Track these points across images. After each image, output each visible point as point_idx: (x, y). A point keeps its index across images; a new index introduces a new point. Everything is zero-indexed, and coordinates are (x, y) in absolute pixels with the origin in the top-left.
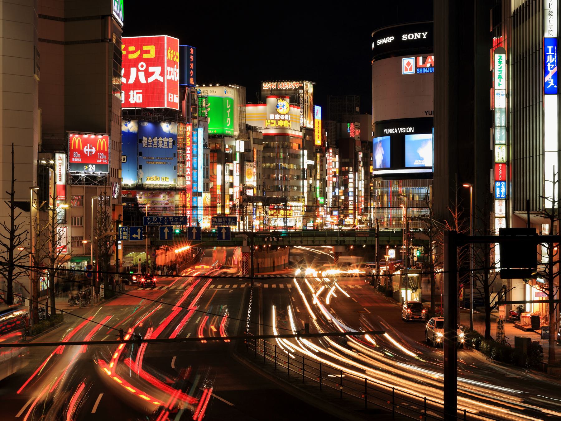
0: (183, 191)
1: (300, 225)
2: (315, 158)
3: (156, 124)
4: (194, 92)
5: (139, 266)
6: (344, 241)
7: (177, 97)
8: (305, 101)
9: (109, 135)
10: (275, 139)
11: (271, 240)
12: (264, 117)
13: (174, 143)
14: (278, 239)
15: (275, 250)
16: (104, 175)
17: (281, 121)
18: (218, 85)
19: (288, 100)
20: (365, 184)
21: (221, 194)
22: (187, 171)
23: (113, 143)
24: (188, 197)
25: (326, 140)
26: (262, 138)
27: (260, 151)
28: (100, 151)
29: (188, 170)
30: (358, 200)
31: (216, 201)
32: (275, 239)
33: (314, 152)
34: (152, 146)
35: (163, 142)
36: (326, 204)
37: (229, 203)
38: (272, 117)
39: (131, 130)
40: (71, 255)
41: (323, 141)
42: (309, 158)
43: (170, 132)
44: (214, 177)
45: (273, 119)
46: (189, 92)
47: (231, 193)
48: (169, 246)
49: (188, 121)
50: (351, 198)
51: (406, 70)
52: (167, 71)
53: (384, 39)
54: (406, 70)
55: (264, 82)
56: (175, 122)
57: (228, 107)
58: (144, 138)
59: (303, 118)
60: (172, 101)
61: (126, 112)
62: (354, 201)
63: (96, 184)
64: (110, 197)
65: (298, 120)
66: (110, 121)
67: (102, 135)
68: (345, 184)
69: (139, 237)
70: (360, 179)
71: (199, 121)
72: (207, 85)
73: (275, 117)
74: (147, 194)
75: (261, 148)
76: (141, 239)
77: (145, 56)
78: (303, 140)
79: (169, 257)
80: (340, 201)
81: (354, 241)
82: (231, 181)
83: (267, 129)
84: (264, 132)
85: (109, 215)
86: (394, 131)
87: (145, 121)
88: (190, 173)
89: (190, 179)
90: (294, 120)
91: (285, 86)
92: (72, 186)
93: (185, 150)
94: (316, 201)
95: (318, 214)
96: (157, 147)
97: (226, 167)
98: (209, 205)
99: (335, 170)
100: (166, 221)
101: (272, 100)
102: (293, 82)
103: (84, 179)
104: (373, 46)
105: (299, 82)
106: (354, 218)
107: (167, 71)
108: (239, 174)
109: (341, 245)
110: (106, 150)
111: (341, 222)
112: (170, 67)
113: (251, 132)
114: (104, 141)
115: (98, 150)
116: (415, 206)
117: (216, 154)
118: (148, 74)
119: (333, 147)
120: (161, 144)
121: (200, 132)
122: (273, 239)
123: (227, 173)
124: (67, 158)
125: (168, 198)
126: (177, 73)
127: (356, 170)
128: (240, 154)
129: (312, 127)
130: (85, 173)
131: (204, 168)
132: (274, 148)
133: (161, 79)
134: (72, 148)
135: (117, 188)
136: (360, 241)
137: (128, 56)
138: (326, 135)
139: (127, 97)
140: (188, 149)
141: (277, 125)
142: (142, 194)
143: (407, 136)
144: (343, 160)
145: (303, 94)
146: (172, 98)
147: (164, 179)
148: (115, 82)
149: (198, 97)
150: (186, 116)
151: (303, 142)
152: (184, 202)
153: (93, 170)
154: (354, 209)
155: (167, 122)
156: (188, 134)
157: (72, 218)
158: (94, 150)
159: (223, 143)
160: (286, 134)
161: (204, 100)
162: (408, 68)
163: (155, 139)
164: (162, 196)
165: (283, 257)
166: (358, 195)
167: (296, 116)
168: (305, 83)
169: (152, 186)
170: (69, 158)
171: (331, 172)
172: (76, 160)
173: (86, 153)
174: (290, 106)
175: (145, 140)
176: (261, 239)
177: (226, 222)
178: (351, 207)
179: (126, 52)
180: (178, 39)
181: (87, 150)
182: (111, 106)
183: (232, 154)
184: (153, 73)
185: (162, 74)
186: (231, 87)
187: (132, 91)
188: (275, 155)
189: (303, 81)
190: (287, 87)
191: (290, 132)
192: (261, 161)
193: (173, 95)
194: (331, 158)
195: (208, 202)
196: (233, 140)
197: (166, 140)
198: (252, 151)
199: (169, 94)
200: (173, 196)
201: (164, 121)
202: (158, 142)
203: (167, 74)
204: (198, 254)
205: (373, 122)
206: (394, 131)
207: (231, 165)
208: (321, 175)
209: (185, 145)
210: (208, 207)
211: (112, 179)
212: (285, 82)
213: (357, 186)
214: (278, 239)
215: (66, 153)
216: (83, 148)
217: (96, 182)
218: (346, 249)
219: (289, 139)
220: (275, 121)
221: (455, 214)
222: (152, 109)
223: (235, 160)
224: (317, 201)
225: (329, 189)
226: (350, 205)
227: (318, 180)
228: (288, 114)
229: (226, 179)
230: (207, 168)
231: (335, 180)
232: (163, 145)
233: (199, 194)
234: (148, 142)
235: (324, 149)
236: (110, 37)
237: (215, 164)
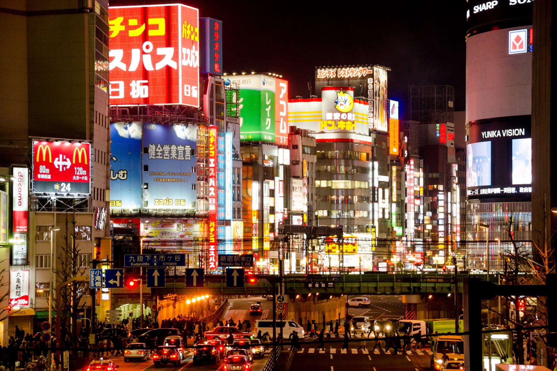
0: (207, 218)
1: (368, 266)
2: (389, 173)
3: (167, 125)
4: (220, 83)
5: (130, 322)
6: (419, 288)
7: (196, 89)
8: (376, 94)
9: (90, 142)
10: (333, 146)
11: (317, 285)
12: (319, 117)
13: (193, 152)
14: (327, 285)
15: (326, 300)
16: (83, 197)
17: (341, 121)
18: (253, 73)
19: (352, 93)
20: (461, 208)
21: (258, 222)
22: (210, 191)
23: (97, 153)
24: (212, 226)
25: (405, 147)
26: (315, 146)
27: (312, 163)
28: (77, 164)
29: (212, 189)
30: (451, 230)
31: (251, 232)
32: (323, 285)
33: (388, 165)
34: (161, 157)
35: (177, 152)
36: (406, 236)
37: (268, 235)
38: (329, 116)
39: (133, 136)
40: (35, 309)
41: (401, 149)
42: (382, 172)
43: (186, 138)
44: (249, 199)
45: (331, 119)
46: (213, 83)
47: (272, 221)
48: (178, 294)
49: (212, 122)
50: (441, 228)
51: (515, 47)
52: (182, 54)
53: (484, 5)
54: (515, 47)
55: (318, 68)
56: (193, 124)
57: (268, 103)
58: (150, 146)
59: (373, 117)
60: (189, 95)
61: (126, 111)
62: (446, 232)
63: (71, 210)
64: (91, 227)
65: (365, 121)
66: (92, 122)
67: (80, 142)
68: (433, 207)
69: (118, 283)
70: (455, 201)
71: (227, 123)
72: (239, 74)
73: (333, 117)
74: (155, 223)
75: (314, 159)
76: (121, 286)
77: (151, 33)
78: (373, 148)
79: (179, 310)
80: (426, 231)
81: (434, 288)
82: (272, 205)
83: (323, 132)
84: (318, 137)
85: (79, 252)
86: (496, 134)
87: (152, 123)
88: (214, 194)
89: (214, 203)
90: (360, 120)
91: (347, 73)
92: (37, 212)
93: (207, 162)
94: (392, 232)
95: (395, 250)
96: (168, 158)
97: (264, 185)
98: (242, 237)
99: (418, 189)
100: (155, 261)
101: (329, 94)
102: (358, 67)
103: (55, 204)
104: (468, 15)
105: (367, 67)
106: (447, 255)
107: (182, 54)
108: (283, 195)
109: (414, 293)
110: (86, 163)
111: (427, 261)
112: (187, 48)
113: (298, 137)
114: (83, 151)
115: (74, 162)
116: (527, 239)
117: (250, 168)
118: (156, 58)
119: (416, 157)
120: (174, 155)
121: (229, 136)
122: (320, 285)
123: (266, 193)
124: (30, 174)
125: (184, 229)
126: (196, 57)
127: (448, 189)
128: (284, 167)
129: (385, 129)
130: (56, 194)
131: (234, 188)
132: (332, 159)
134: (38, 160)
135: (104, 214)
136: (442, 288)
137: (128, 33)
138: (406, 141)
139: (128, 89)
140: (212, 160)
141: (336, 128)
142: (148, 223)
143: (514, 141)
144: (430, 175)
145: (373, 84)
146: (189, 90)
147: (179, 201)
148: (99, 66)
149: (226, 90)
150: (208, 116)
151: (372, 151)
152: (206, 233)
153: (67, 191)
154: (446, 242)
155: (183, 125)
156: (212, 140)
157: (37, 257)
158: (68, 164)
159: (260, 153)
160: (349, 139)
161: (234, 95)
162: (518, 45)
163: (166, 148)
164: (175, 225)
165: (337, 309)
166: (451, 224)
167: (363, 114)
168: (375, 68)
169: (162, 212)
170: (34, 174)
171: (412, 191)
172: (43, 176)
173: (57, 167)
174: (355, 101)
175: (152, 149)
176: (303, 285)
177: (238, 262)
178: (441, 240)
179: (126, 28)
180: (198, 10)
181: (58, 163)
182: (93, 103)
183: (273, 168)
185: (175, 58)
186: (271, 75)
187: (133, 82)
188: (333, 169)
189: (372, 66)
190: (351, 75)
191: (353, 137)
192: (314, 176)
193: (191, 87)
194: (412, 172)
195: (240, 235)
196: (274, 149)
197: (181, 148)
198: (301, 164)
199: (186, 86)
200: (191, 225)
201: (179, 122)
202: (170, 152)
203: (182, 58)
204: (223, 306)
205: (467, 122)
206: (496, 134)
207: (271, 182)
208: (398, 196)
209: (208, 156)
210: (240, 241)
211: (95, 203)
212: (348, 69)
213: (449, 212)
214: (327, 285)
215: (29, 167)
216: (53, 160)
217: (72, 207)
218: (422, 298)
219: (352, 146)
220: (333, 122)
221: (544, 252)
222: (162, 107)
223: (278, 176)
224: (393, 232)
225: (410, 216)
226: (441, 237)
227: (394, 202)
228: (351, 112)
229: (265, 202)
230: (239, 188)
231: (418, 202)
232: (177, 156)
233: (228, 223)
234: (156, 152)
235: (402, 160)
236: (90, 5)
237: (249, 181)
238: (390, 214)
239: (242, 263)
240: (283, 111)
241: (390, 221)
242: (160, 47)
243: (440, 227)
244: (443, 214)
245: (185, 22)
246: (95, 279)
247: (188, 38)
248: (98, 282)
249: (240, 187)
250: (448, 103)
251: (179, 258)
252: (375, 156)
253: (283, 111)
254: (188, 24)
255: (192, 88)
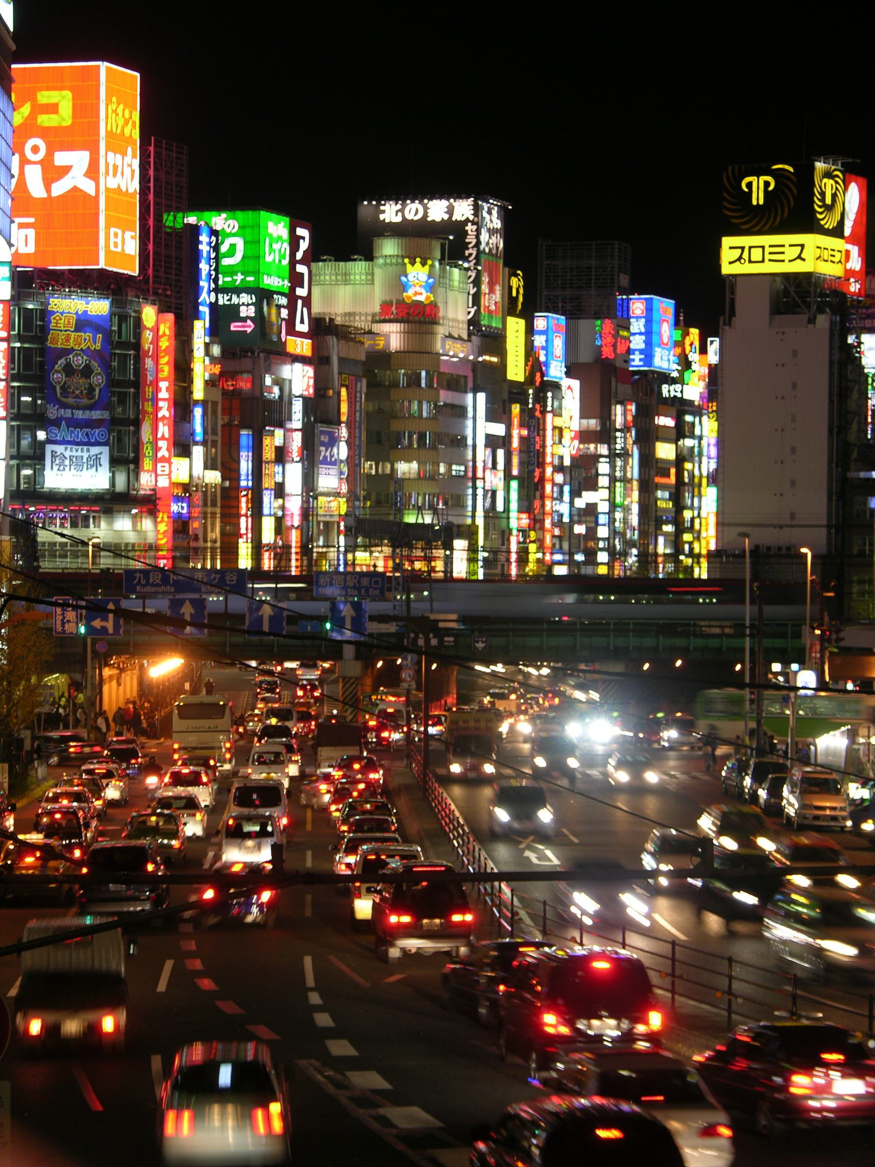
7: (132, 237)
52: (107, 165)
60: (119, 249)
77: (45, 120)
107: (107, 165)
113: (332, 341)
126: (133, 171)
133: (88, 187)
146: (119, 240)
177: (354, 587)
184: (66, 170)
185: (92, 172)
193: (124, 233)
203: (107, 173)
238: (507, 501)
239: (363, 591)
240: (302, 287)
241: (505, 515)
242: (61, 150)
243: (599, 528)
244: (607, 503)
245: (114, 99)
246: (64, 618)
247: (119, 131)
248: (70, 624)
249: (216, 441)
250: (619, 279)
251: (235, 578)
252: (479, 382)
253: (302, 287)
254: (119, 104)
255: (125, 236)
